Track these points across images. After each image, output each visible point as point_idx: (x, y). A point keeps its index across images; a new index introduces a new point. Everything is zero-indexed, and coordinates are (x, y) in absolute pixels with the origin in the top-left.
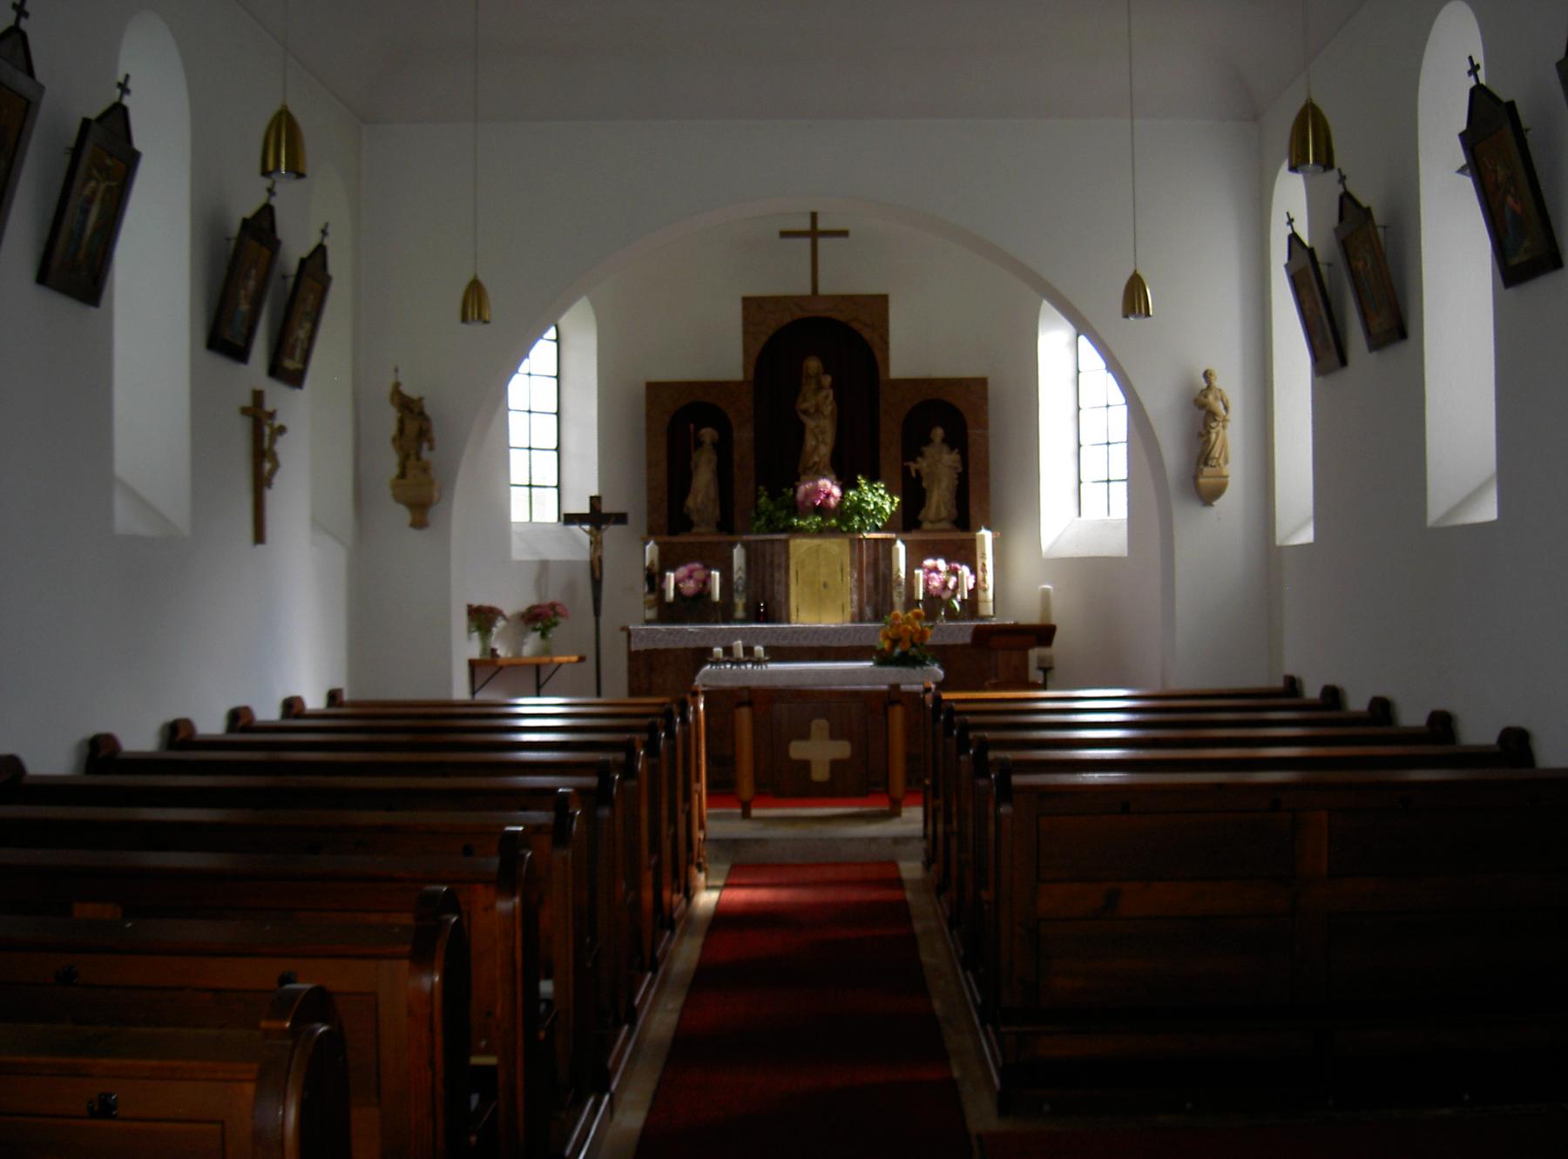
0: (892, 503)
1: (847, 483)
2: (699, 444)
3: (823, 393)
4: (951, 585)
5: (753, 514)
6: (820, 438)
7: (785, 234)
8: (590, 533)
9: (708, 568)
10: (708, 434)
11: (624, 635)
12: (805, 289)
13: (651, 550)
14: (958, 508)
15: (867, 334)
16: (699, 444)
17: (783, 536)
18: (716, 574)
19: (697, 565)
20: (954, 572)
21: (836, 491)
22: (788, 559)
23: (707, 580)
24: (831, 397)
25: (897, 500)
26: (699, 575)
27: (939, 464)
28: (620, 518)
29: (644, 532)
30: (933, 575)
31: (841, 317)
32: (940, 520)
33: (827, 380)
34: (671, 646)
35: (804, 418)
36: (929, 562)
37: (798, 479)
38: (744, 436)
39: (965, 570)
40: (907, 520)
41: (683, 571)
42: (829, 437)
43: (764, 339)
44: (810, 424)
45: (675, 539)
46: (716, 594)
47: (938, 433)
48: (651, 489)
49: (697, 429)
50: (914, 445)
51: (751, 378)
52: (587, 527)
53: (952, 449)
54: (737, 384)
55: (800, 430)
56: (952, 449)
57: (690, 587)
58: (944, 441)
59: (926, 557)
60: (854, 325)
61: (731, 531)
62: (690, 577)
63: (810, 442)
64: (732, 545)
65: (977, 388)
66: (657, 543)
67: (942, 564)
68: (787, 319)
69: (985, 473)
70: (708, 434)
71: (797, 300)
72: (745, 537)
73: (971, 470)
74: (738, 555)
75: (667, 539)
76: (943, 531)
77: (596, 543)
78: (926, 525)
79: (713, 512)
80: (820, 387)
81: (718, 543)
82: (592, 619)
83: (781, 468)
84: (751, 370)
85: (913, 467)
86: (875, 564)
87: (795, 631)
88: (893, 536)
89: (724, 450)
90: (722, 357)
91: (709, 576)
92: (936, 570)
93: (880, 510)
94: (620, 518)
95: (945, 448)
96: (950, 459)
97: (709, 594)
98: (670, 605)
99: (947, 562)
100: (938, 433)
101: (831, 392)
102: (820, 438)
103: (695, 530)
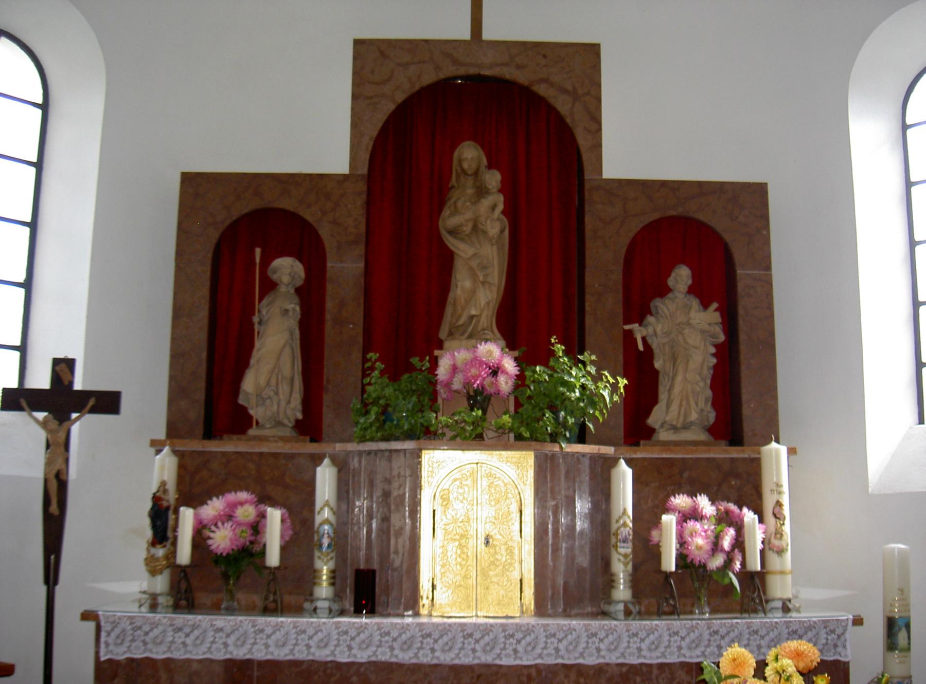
0: (614, 388)
1: (531, 352)
2: (269, 286)
3: (486, 202)
4: (726, 543)
5: (356, 404)
6: (478, 278)
7: (434, 511)
8: (44, 424)
9: (265, 499)
10: (287, 269)
11: (91, 625)
12: (465, 34)
13: (163, 468)
14: (716, 403)
15: (562, 105)
16: (269, 286)
17: (409, 445)
18: (275, 515)
19: (243, 495)
20: (725, 519)
21: (510, 365)
22: (416, 487)
23: (257, 527)
24: (501, 207)
25: (623, 382)
26: (247, 513)
27: (682, 329)
28: (107, 403)
29: (161, 433)
30: (691, 524)
31: (522, 78)
32: (686, 427)
33: (493, 179)
34: (178, 655)
35: (451, 242)
36: (681, 501)
37: (440, 345)
38: (346, 268)
39: (749, 516)
40: (635, 425)
41: (213, 508)
42: (496, 275)
43: (389, 107)
44: (462, 250)
45: (214, 446)
46: (273, 558)
47: (681, 277)
48: (177, 356)
49: (266, 261)
50: (640, 298)
51: (364, 170)
52: (41, 415)
53: (705, 305)
54: (341, 179)
55: (445, 261)
56: (705, 305)
57: (222, 539)
58: (691, 290)
59: (678, 491)
60: (542, 90)
61: (316, 438)
62: (228, 516)
63: (462, 283)
64: (317, 460)
65: (751, 199)
66: (175, 452)
67: (704, 503)
68: (429, 78)
69: (767, 344)
70: (287, 269)
71: (447, 47)
72: (339, 447)
73: (742, 337)
74: (325, 479)
75: (196, 445)
76: (695, 443)
77: (58, 447)
78: (664, 435)
79: (292, 406)
80: (481, 192)
81: (291, 457)
82: (42, 590)
83: (406, 326)
84: (365, 156)
85: (639, 332)
86: (58, 475)
87: (427, 633)
88: (609, 450)
89: (311, 296)
90: (311, 133)
91: (263, 515)
92: (694, 515)
93: (592, 399)
94: (107, 403)
95: (695, 303)
96: (705, 321)
97: (263, 553)
98: (183, 569)
99: (713, 501)
100: (681, 277)
101: (501, 198)
102: (478, 278)
103: (252, 432)
